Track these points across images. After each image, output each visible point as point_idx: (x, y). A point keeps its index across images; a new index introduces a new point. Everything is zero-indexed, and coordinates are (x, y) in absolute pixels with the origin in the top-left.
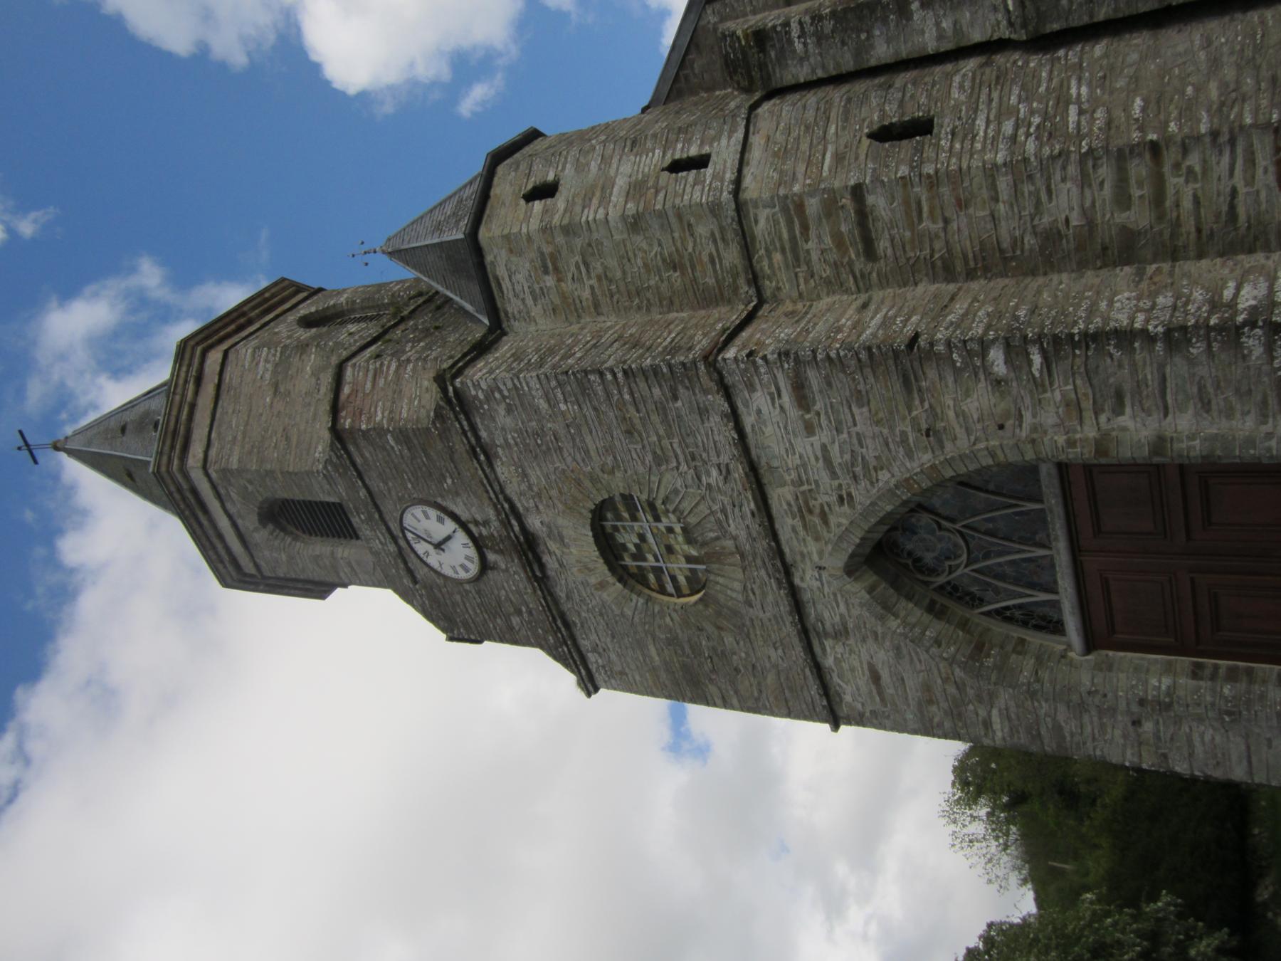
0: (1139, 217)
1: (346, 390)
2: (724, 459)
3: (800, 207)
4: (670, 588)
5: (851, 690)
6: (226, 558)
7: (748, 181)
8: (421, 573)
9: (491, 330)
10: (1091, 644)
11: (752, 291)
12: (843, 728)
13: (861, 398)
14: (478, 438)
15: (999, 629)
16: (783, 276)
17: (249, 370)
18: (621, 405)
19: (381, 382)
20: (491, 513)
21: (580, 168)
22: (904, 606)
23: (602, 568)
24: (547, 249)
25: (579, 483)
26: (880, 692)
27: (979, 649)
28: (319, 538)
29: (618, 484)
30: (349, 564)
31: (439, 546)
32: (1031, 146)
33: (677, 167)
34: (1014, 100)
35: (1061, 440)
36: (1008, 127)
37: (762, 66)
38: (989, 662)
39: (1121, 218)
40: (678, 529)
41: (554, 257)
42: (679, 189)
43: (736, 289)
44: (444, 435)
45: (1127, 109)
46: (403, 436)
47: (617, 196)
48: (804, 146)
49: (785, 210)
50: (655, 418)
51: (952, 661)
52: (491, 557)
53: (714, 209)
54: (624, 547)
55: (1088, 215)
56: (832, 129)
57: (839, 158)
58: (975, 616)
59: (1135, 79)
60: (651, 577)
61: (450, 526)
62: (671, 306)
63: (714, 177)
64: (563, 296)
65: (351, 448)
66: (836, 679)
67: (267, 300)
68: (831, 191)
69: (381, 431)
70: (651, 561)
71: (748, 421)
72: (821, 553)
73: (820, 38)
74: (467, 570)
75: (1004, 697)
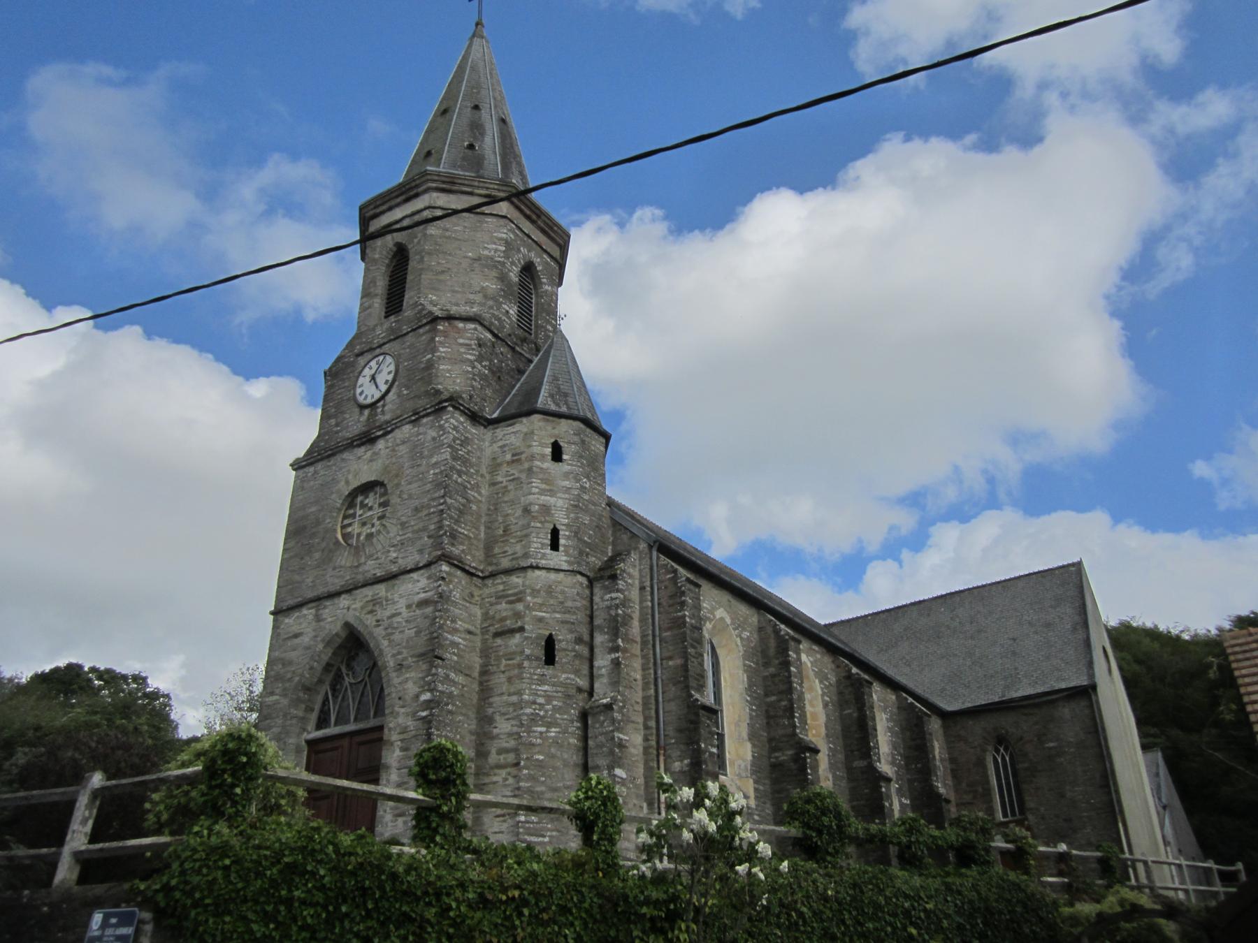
0: (493, 758)
1: (461, 325)
2: (400, 561)
3: (519, 600)
4: (346, 522)
5: (289, 621)
6: (378, 211)
7: (538, 572)
8: (362, 360)
9: (487, 420)
10: (310, 743)
11: (487, 574)
12: (272, 617)
13: (418, 633)
14: (423, 416)
15: (319, 699)
16: (493, 590)
17: (492, 237)
18: (429, 507)
19: (462, 350)
20: (388, 417)
21: (566, 475)
22: (330, 651)
23: (355, 484)
24: (523, 456)
25: (397, 476)
26: (289, 638)
27: (307, 689)
28: (387, 283)
29: (394, 500)
30: (370, 307)
31: (373, 378)
32: (528, 711)
33: (555, 533)
34: (555, 703)
35: (391, 725)
36: (541, 700)
37: (602, 578)
38: (301, 694)
39: (494, 751)
40: (373, 530)
41: (518, 461)
42: (541, 535)
43: (490, 564)
44: (427, 393)
45: (539, 753)
46: (430, 365)
47: (545, 499)
48: (552, 602)
49: (521, 592)
50: (421, 525)
51: (302, 675)
52: (366, 412)
53: (526, 555)
54: (367, 497)
55: (497, 737)
56: (558, 616)
57: (541, 620)
58: (326, 687)
59: (553, 756)
60: (351, 512)
61: (384, 388)
62: (488, 528)
63: (544, 555)
64: (500, 465)
65: (427, 328)
66: (297, 614)
67: (551, 228)
68: (523, 617)
69: (434, 350)
70: (359, 512)
71: (415, 575)
72: (355, 609)
73: (609, 608)
74: (361, 394)
75: (285, 702)
